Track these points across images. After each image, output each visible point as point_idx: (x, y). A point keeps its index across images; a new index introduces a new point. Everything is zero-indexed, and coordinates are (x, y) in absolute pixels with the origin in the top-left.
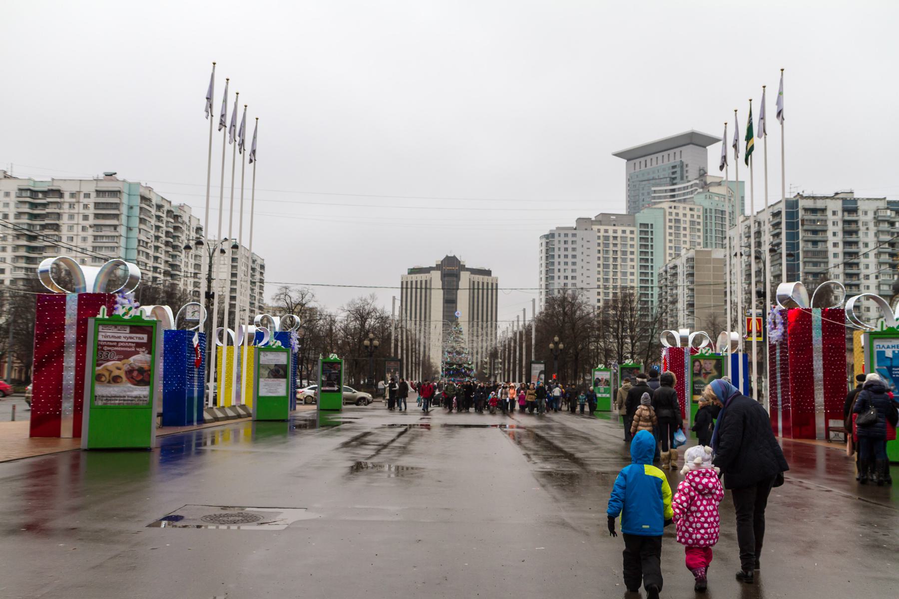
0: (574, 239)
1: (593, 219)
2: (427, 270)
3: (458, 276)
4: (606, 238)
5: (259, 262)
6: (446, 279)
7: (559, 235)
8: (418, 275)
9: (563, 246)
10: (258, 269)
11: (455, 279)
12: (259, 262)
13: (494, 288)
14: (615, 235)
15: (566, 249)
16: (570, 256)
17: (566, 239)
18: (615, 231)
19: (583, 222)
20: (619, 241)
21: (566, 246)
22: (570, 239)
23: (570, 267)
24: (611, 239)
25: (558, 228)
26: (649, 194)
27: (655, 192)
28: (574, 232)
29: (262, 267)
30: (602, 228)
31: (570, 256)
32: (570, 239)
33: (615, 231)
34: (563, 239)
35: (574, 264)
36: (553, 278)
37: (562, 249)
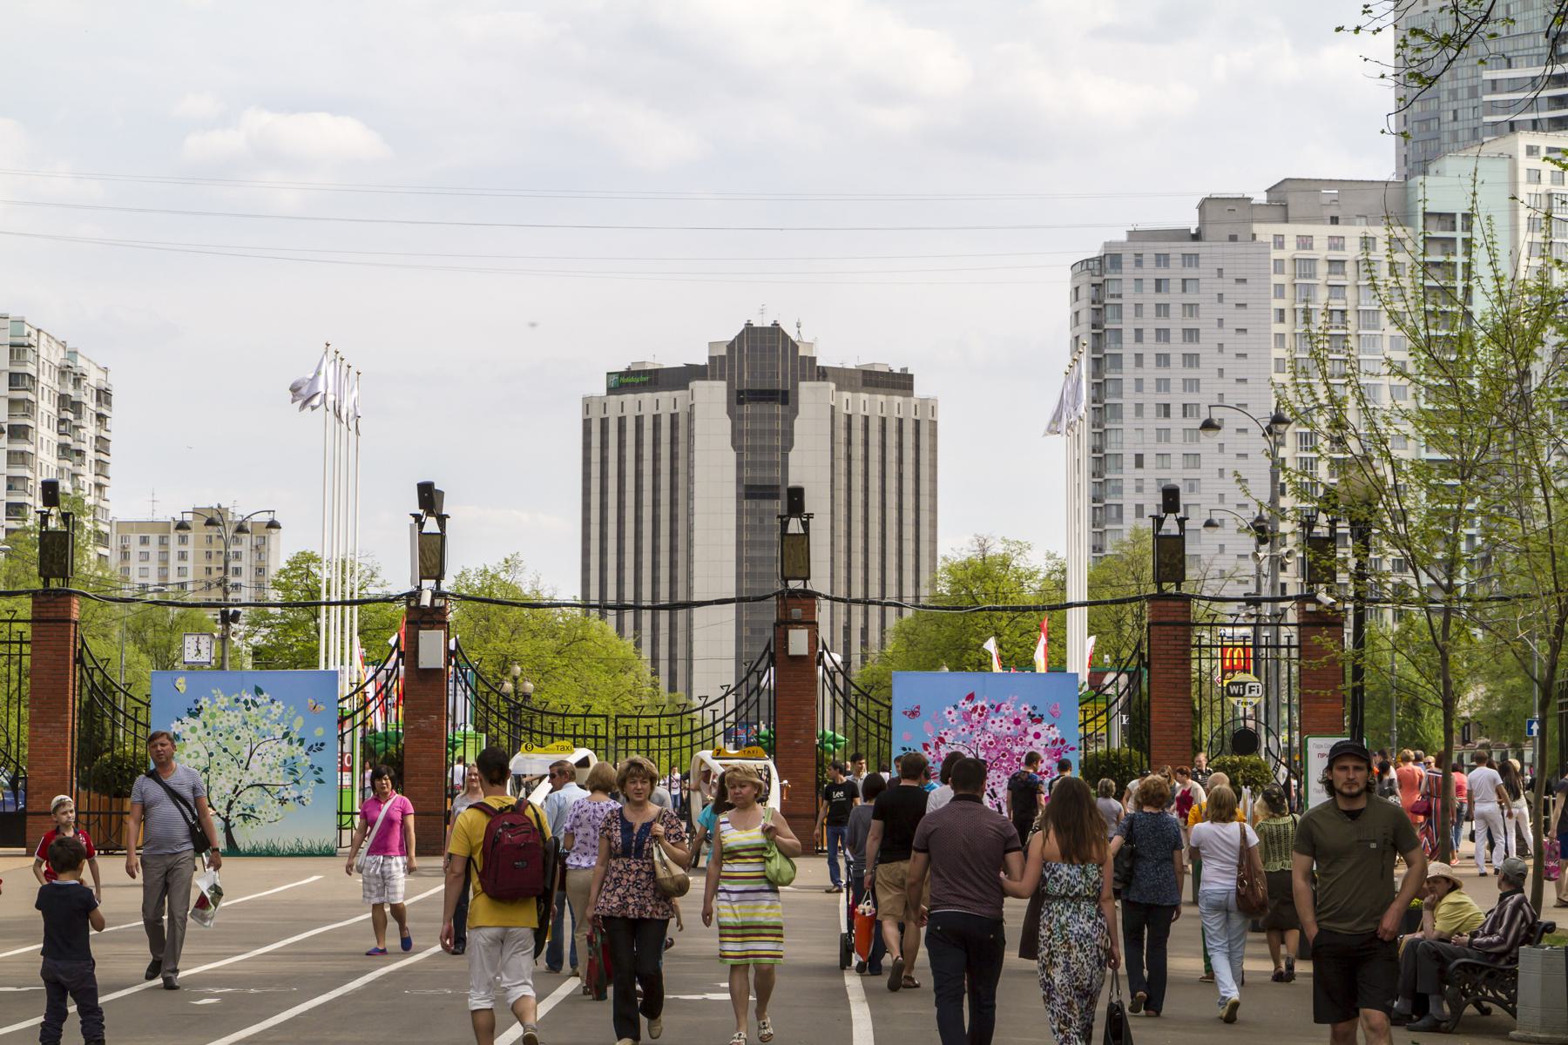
0: (1190, 273)
1: (1261, 198)
2: (680, 378)
3: (785, 398)
4: (1305, 267)
5: (93, 379)
6: (747, 409)
7: (1139, 261)
8: (647, 398)
9: (1150, 298)
10: (91, 404)
11: (779, 409)
12: (93, 379)
13: (920, 435)
14: (1336, 255)
15: (1162, 310)
16: (1176, 335)
17: (1162, 273)
18: (1336, 243)
19: (1224, 216)
20: (1349, 278)
21: (1162, 298)
22: (1175, 272)
23: (1177, 372)
24: (1322, 269)
25: (1134, 235)
26: (1473, 92)
27: (1494, 85)
28: (1191, 247)
29: (103, 395)
30: (1291, 231)
31: (1176, 335)
32: (1175, 272)
33: (1336, 243)
34: (1150, 272)
35: (1191, 360)
36: (1117, 410)
37: (1149, 310)
